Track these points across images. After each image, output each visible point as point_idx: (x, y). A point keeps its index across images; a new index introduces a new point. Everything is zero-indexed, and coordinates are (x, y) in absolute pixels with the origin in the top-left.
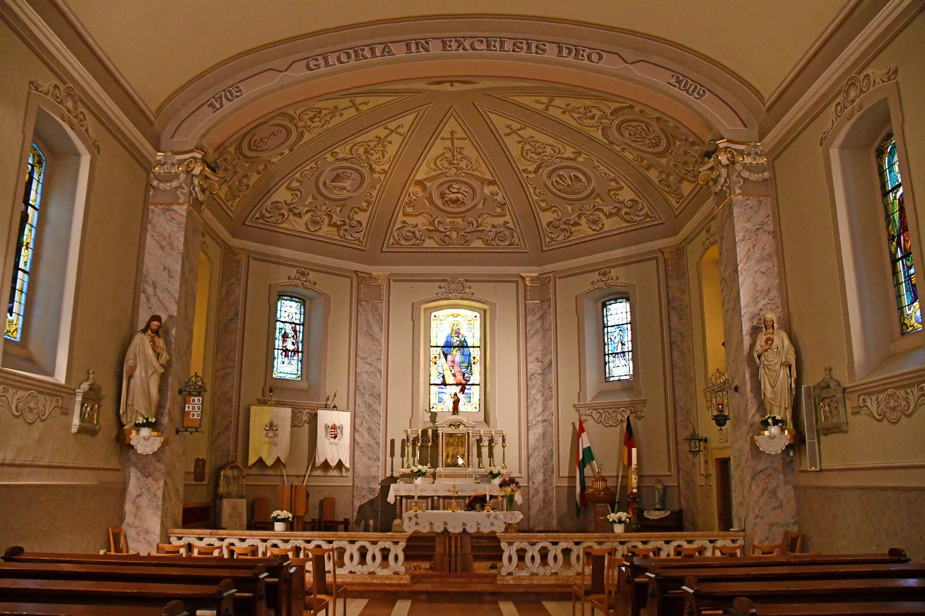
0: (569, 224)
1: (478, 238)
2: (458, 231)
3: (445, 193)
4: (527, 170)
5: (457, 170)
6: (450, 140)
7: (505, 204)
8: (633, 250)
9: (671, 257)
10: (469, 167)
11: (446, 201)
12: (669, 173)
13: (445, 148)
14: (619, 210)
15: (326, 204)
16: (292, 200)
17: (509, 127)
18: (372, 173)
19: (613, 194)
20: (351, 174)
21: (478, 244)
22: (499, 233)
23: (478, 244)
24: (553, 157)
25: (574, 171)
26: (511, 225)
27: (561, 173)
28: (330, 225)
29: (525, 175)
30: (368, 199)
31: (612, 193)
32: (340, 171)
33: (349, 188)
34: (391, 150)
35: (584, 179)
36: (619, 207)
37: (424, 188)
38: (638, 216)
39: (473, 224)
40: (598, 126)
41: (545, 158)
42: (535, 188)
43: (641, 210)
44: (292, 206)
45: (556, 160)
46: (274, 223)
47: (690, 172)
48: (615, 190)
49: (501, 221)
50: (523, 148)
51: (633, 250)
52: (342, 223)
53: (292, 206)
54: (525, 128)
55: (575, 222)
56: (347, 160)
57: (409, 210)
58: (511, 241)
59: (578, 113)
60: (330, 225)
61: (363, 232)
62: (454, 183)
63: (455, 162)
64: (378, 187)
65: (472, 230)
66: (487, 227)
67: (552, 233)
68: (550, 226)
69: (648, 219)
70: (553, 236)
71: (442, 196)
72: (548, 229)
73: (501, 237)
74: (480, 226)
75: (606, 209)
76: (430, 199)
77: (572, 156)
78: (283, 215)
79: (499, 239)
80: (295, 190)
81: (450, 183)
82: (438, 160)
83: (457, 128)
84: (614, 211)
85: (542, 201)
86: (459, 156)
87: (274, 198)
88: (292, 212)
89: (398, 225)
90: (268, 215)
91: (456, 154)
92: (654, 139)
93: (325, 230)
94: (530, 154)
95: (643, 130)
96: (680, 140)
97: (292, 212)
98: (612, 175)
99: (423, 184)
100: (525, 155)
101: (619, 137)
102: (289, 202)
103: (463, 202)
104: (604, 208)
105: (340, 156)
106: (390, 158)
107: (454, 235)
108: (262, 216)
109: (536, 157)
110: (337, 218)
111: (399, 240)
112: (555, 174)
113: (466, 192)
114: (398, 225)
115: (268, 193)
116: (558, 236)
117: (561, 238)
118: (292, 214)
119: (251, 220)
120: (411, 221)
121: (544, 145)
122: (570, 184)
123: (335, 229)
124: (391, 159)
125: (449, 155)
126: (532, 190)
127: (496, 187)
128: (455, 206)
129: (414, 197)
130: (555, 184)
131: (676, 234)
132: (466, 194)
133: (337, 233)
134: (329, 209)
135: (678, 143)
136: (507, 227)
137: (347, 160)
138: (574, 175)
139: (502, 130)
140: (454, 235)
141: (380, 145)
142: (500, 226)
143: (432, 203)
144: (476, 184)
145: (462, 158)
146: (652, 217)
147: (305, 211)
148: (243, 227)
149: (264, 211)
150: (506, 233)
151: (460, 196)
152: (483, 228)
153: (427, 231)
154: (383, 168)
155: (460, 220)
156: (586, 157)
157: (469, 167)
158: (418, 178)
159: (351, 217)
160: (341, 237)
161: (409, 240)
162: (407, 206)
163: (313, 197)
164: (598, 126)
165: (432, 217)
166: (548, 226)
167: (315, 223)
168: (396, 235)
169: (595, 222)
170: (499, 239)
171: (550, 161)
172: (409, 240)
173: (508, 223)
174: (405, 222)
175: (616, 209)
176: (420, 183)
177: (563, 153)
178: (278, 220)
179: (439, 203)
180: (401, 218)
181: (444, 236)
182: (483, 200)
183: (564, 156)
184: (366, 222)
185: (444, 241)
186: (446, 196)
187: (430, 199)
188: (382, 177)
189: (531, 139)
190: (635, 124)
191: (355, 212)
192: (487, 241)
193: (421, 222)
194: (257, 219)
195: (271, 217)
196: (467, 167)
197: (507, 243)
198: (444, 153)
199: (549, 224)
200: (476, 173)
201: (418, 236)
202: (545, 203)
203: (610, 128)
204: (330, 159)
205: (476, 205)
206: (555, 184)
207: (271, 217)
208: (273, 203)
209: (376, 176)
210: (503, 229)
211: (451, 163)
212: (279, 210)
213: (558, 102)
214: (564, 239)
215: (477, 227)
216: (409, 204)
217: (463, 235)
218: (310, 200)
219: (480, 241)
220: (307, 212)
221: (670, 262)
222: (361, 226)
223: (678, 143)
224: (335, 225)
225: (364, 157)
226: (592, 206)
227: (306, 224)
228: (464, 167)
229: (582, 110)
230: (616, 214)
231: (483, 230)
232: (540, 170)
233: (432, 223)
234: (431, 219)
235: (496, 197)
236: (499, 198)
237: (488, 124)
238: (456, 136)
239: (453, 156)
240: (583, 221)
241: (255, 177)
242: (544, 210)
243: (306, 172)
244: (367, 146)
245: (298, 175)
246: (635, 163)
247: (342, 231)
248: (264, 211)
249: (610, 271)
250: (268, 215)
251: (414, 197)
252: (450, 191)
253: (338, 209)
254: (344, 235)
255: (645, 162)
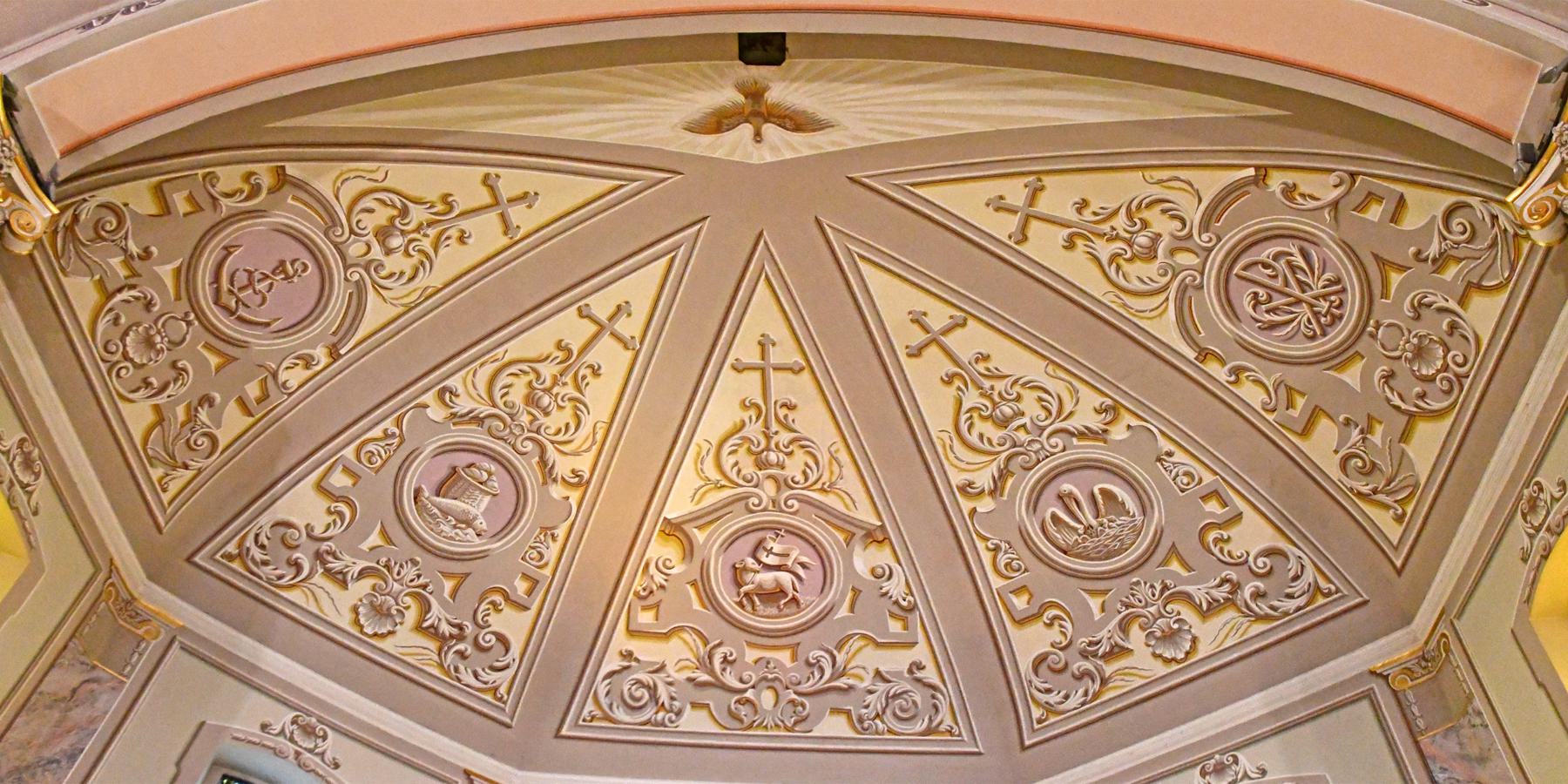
0: (1095, 655)
1: (836, 711)
2: (777, 685)
3: (745, 569)
4: (970, 484)
5: (779, 489)
6: (757, 375)
7: (912, 609)
8: (1292, 690)
9: (1410, 683)
10: (812, 479)
11: (746, 594)
12: (1370, 418)
13: (745, 406)
14: (1236, 587)
15: (415, 563)
16: (328, 526)
17: (918, 320)
18: (545, 483)
19: (1216, 541)
20: (490, 474)
21: (834, 726)
22: (896, 696)
23: (834, 726)
24: (1043, 429)
25: (1104, 475)
26: (930, 675)
27: (1067, 487)
28: (419, 628)
29: (966, 505)
30: (530, 568)
31: (1212, 536)
32: (462, 459)
33: (481, 523)
34: (601, 396)
35: (1131, 505)
36: (1234, 576)
37: (689, 550)
38: (1290, 596)
39: (822, 670)
40: (1165, 288)
41: (1022, 436)
42: (997, 549)
43: (1296, 578)
44: (324, 546)
45: (1053, 441)
46: (269, 581)
47: (1431, 379)
48: (1219, 526)
49: (896, 661)
50: (960, 403)
51: (1292, 690)
52: (455, 631)
53: (324, 546)
54: (964, 324)
55: (1112, 647)
56: (479, 420)
57: (645, 618)
58: (931, 720)
59: (1111, 239)
60: (419, 628)
61: (510, 673)
62: (770, 534)
63: (773, 457)
64: (561, 532)
65: (819, 686)
66: (861, 679)
67: (1048, 691)
68: (1043, 669)
69: (1321, 601)
70: (1053, 698)
71: (737, 575)
72: (1036, 682)
73: (903, 710)
74: (842, 675)
75: (1199, 592)
76: (702, 584)
77: (1095, 422)
78: (298, 567)
79: (895, 714)
80: (337, 499)
81: (760, 535)
82: (726, 449)
83: (779, 331)
84: (1220, 594)
85: (1017, 591)
86: (785, 437)
87: (280, 511)
88: (324, 563)
89: (612, 663)
90: (257, 553)
91: (774, 427)
92: (1325, 297)
93: (405, 641)
94: (980, 426)
95: (1293, 268)
96: (1402, 268)
97: (324, 563)
98: (1208, 478)
99: (687, 536)
100: (964, 427)
101: (1226, 325)
102: (318, 532)
103: (794, 599)
104: (1190, 589)
105: (464, 405)
106: (594, 434)
107: (767, 699)
108: (243, 554)
109: (995, 434)
110: (444, 614)
111: (611, 706)
112: (1050, 493)
113: (803, 565)
114: (612, 663)
115: (266, 491)
116: (1067, 697)
117: (1073, 702)
118: (321, 571)
119: (212, 557)
120: (646, 651)
121: (1017, 388)
122: (1094, 522)
123: (433, 645)
124: (599, 437)
125: (754, 430)
126: (986, 557)
127: (887, 551)
128: (774, 611)
129: (659, 578)
130: (1051, 528)
131: (1407, 620)
132: (801, 571)
133: (436, 658)
134: (422, 581)
135: (1395, 278)
136: (918, 680)
137: (479, 420)
138: (1103, 491)
139: (906, 336)
140: (767, 699)
141: (568, 379)
142: (899, 674)
143: (710, 600)
144: (830, 539)
145: (791, 442)
146: (1329, 594)
147: (357, 569)
148: (186, 565)
149: (250, 542)
150: (918, 699)
151: (785, 578)
152: (851, 682)
153: (690, 686)
154: (577, 467)
155: (784, 656)
156: (1135, 422)
157: (812, 479)
158: (671, 513)
159: (480, 616)
160: (447, 673)
161: (641, 708)
162: (638, 604)
163: (384, 532)
164: (1165, 288)
165: (706, 642)
166: (1036, 671)
167: (380, 612)
168: (602, 691)
169: (1170, 637)
170: (895, 714)
171: (1036, 446)
172: (641, 708)
173: (921, 667)
174: (628, 655)
175: (1227, 587)
176: (674, 529)
177: (1071, 413)
178: (280, 577)
179: (728, 600)
180: (621, 641)
181: (738, 702)
182: (850, 595)
183: (1074, 424)
184: (523, 638)
185: (735, 716)
186: (749, 577)
187: (702, 584)
188: (574, 496)
189: (981, 367)
190: (1267, 252)
191: (493, 603)
192: (861, 721)
193: (676, 655)
194: (230, 557)
195: (265, 563)
196: (806, 479)
197: (920, 726)
198: (743, 424)
199: (1039, 661)
200: (830, 500)
201: (664, 697)
202: (1025, 597)
203: (1200, 287)
204: (436, 413)
205: (830, 610)
206: (1051, 528)
207: (265, 563)
208: (278, 524)
209: (557, 491)
210: (909, 687)
211: (761, 464)
212: (290, 548)
213: (1058, 197)
214: (1083, 704)
215: (829, 681)
216: (644, 597)
217: (792, 702)
218: (375, 539)
219: (842, 720)
220: (363, 574)
221: (1411, 697)
222: (507, 650)
223: (1395, 278)
224: (433, 632)
225: (525, 419)
226: (1158, 587)
227: (355, 610)
228: (799, 478)
229: (1120, 222)
230: (1230, 602)
231: (851, 688)
232: (1010, 482)
233: (705, 663)
234: (702, 651)
235: (887, 586)
236: (896, 587)
237: (861, 308)
238: (775, 357)
239: (768, 437)
240: (1137, 636)
241: (233, 422)
242: (1021, 622)
243: (371, 447)
244: (532, 376)
245: (349, 452)
246: (1270, 417)
247: (451, 655)
248: (250, 542)
249: (1235, 757)
250: (257, 553)
251: (659, 578)
252: (759, 562)
253: (449, 585)
254: (456, 669)
255: (1300, 402)
